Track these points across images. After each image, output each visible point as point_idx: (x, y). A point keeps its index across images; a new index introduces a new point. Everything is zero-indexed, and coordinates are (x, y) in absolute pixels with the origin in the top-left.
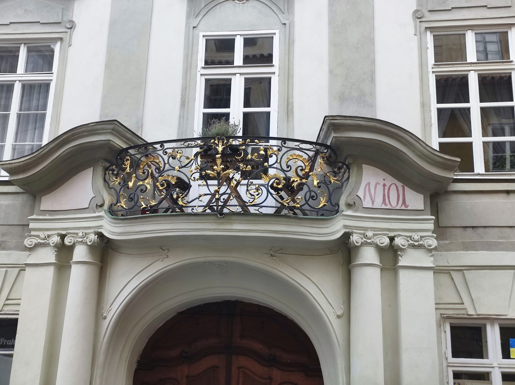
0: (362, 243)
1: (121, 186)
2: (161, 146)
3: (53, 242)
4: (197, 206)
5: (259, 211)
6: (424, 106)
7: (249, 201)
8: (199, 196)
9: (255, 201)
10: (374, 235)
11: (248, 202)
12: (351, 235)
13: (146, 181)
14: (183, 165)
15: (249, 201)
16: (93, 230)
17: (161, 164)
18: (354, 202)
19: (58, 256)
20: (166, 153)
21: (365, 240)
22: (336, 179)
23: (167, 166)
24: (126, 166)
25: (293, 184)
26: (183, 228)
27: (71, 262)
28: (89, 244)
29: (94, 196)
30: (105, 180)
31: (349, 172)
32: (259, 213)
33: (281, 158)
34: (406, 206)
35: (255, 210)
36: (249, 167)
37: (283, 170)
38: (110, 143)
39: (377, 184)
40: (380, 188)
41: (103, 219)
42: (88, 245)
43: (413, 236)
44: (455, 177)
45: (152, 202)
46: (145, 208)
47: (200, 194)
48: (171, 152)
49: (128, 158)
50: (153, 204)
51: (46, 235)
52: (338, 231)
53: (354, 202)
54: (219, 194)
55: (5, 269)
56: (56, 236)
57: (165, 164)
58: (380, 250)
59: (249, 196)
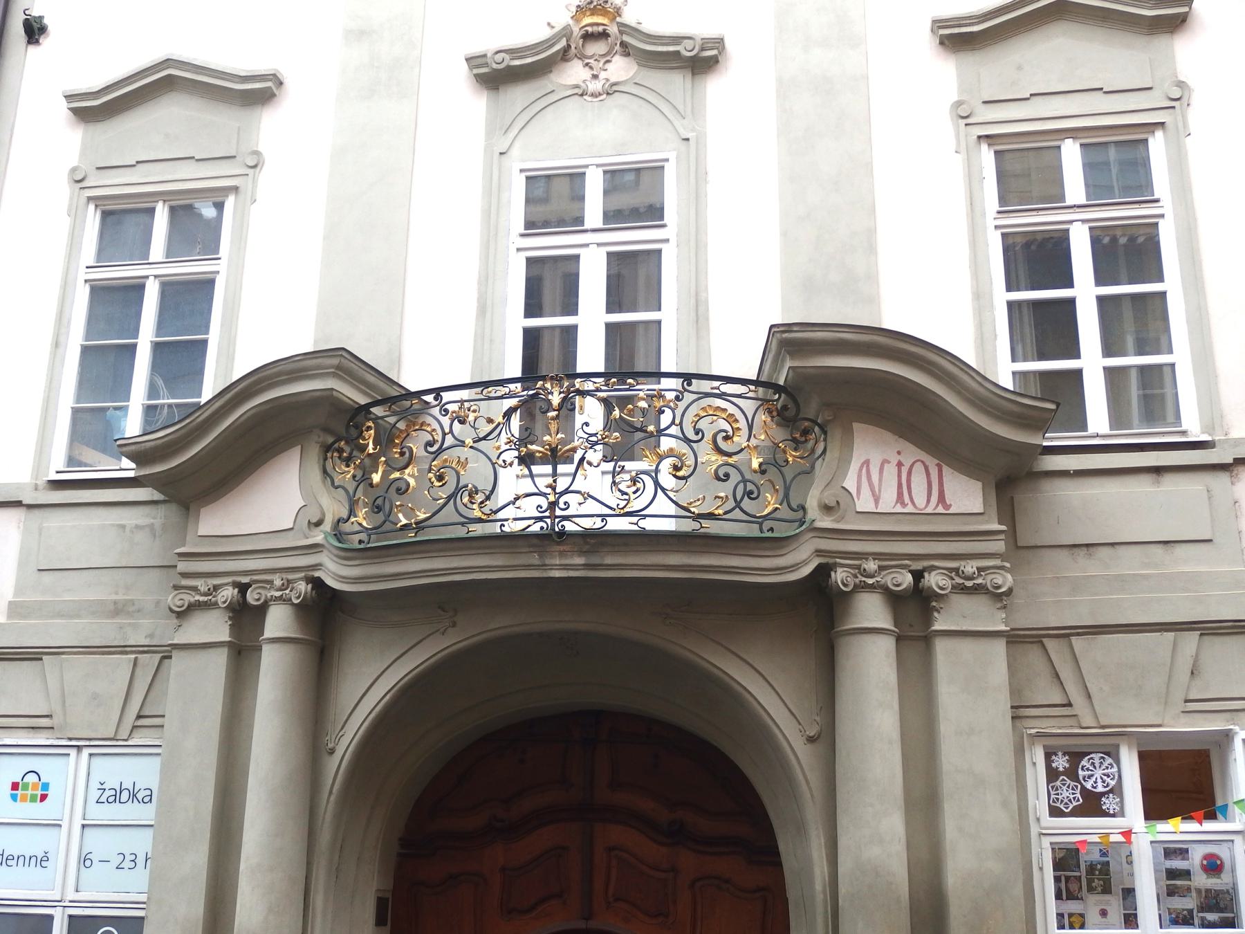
0: (855, 586)
2: (436, 399)
3: (223, 600)
6: (981, 297)
7: (618, 505)
8: (515, 498)
10: (881, 568)
11: (616, 508)
12: (832, 570)
13: (407, 471)
14: (481, 435)
15: (618, 505)
16: (303, 575)
18: (837, 502)
19: (234, 628)
20: (446, 411)
21: (864, 579)
22: (798, 454)
24: (366, 442)
27: (832, 632)
28: (296, 601)
29: (304, 504)
30: (325, 472)
33: (683, 415)
34: (947, 507)
37: (687, 441)
39: (885, 462)
40: (891, 470)
41: (322, 551)
42: (293, 604)
43: (962, 568)
44: (1045, 444)
45: (418, 513)
46: (405, 525)
49: (370, 424)
50: (422, 516)
51: (211, 586)
52: (805, 563)
53: (837, 502)
54: (556, 493)
55: (133, 656)
56: (231, 588)
57: (444, 434)
58: (895, 599)
59: (618, 494)
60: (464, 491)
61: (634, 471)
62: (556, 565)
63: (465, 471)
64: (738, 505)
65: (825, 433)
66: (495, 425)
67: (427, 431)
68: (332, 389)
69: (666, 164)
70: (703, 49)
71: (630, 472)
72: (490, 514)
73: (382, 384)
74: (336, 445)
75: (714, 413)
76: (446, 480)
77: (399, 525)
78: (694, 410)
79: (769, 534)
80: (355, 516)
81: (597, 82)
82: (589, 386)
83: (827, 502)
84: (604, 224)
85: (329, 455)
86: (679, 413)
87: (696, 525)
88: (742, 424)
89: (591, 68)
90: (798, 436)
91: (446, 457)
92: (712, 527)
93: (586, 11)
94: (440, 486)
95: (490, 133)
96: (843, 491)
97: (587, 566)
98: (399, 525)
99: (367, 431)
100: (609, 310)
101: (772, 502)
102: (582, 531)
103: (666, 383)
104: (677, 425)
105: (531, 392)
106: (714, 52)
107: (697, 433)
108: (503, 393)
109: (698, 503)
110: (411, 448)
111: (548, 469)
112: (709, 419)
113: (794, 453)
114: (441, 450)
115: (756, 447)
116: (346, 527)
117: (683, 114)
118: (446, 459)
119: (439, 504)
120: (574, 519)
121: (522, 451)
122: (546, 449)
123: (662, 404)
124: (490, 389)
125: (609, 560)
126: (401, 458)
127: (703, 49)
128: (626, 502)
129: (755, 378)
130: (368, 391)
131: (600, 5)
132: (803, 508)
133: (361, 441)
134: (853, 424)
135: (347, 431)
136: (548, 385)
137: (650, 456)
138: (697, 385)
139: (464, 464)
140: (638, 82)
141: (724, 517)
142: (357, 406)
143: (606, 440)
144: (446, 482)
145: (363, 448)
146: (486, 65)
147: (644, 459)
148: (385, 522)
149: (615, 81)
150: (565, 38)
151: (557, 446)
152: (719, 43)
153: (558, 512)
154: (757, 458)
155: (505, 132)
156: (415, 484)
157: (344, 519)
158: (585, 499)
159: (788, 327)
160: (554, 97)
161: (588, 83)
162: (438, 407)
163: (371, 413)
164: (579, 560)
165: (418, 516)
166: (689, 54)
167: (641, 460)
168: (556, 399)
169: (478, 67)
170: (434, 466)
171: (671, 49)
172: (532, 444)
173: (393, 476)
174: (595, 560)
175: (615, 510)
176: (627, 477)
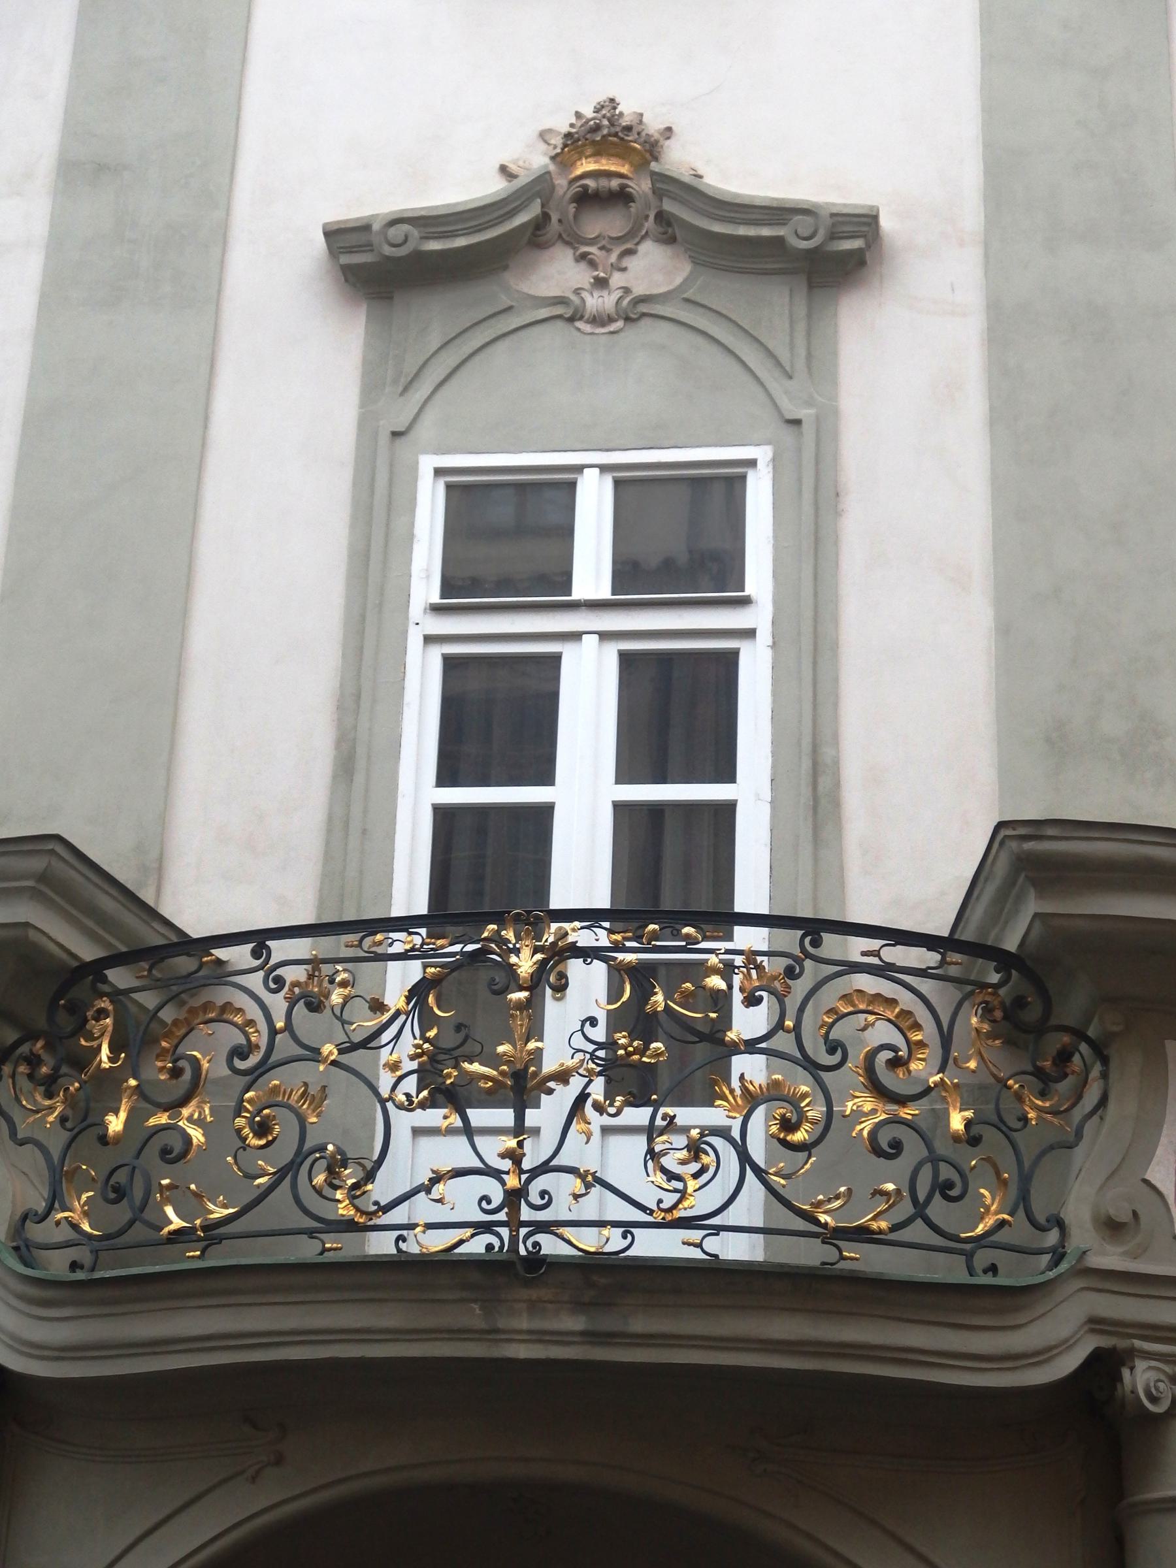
2: (256, 954)
7: (660, 1201)
8: (430, 1180)
9: (686, 1204)
11: (655, 1208)
12: (1123, 1365)
13: (186, 1112)
14: (357, 1038)
15: (660, 1201)
17: (257, 1031)
18: (1135, 1214)
20: (280, 981)
22: (1047, 1104)
24: (95, 1044)
26: (359, 1325)
33: (801, 1010)
36: (657, 1049)
37: (812, 1067)
45: (211, 1206)
46: (179, 1232)
47: (433, 1172)
49: (105, 1004)
50: (219, 1213)
52: (1065, 1346)
53: (1135, 1214)
57: (273, 1032)
59: (660, 1178)
60: (317, 1159)
61: (695, 1127)
62: (520, 1332)
63: (318, 1116)
64: (920, 1211)
65: (1105, 1061)
66: (386, 1017)
67: (235, 1025)
68: (27, 925)
69: (436, 598)
70: (833, 236)
71: (686, 1130)
72: (374, 1213)
73: (130, 919)
74: (24, 1049)
77: (166, 1230)
78: (830, 996)
79: (988, 1280)
80: (64, 1209)
81: (605, 293)
82: (584, 937)
83: (1112, 1212)
84: (613, 594)
87: (830, 1254)
88: (928, 1032)
89: (593, 264)
90: (1047, 1064)
91: (277, 1082)
93: (584, 145)
95: (371, 389)
96: (1146, 1189)
97: (591, 1337)
98: (166, 1230)
99: (97, 1020)
100: (624, 775)
101: (993, 1208)
102: (580, 1256)
103: (748, 938)
104: (788, 1031)
105: (470, 948)
106: (857, 244)
107: (831, 1051)
108: (408, 947)
109: (837, 1204)
111: (505, 1117)
113: (1039, 1103)
114: (264, 1068)
115: (956, 1086)
116: (37, 1233)
117: (788, 368)
118: (275, 1086)
119: (258, 1186)
120: (561, 1230)
121: (449, 1076)
122: (503, 1073)
124: (379, 937)
125: (638, 1325)
126: (174, 1081)
127: (833, 236)
128: (678, 1195)
129: (945, 933)
130: (101, 932)
131: (616, 135)
132: (1060, 1224)
133: (83, 1042)
134: (1167, 1042)
135: (51, 1019)
136: (509, 934)
138: (832, 946)
139: (317, 1099)
140: (693, 298)
141: (892, 1236)
142: (75, 964)
144: (275, 1139)
145: (82, 1061)
146: (368, 247)
147: (718, 1102)
148: (131, 1223)
149: (641, 293)
150: (539, 200)
151: (526, 1068)
152: (869, 224)
153: (526, 1214)
154: (961, 1110)
155: (406, 389)
156: (202, 1139)
157: (36, 1214)
158: (588, 1186)
159: (1036, 828)
160: (515, 321)
161: (585, 295)
162: (261, 974)
163: (105, 980)
164: (574, 1323)
165: (212, 1212)
166: (804, 245)
167: (712, 1105)
168: (525, 963)
169: (350, 250)
171: (766, 232)
173: (152, 1122)
174: (607, 1322)
175: (651, 1212)
176: (680, 1141)
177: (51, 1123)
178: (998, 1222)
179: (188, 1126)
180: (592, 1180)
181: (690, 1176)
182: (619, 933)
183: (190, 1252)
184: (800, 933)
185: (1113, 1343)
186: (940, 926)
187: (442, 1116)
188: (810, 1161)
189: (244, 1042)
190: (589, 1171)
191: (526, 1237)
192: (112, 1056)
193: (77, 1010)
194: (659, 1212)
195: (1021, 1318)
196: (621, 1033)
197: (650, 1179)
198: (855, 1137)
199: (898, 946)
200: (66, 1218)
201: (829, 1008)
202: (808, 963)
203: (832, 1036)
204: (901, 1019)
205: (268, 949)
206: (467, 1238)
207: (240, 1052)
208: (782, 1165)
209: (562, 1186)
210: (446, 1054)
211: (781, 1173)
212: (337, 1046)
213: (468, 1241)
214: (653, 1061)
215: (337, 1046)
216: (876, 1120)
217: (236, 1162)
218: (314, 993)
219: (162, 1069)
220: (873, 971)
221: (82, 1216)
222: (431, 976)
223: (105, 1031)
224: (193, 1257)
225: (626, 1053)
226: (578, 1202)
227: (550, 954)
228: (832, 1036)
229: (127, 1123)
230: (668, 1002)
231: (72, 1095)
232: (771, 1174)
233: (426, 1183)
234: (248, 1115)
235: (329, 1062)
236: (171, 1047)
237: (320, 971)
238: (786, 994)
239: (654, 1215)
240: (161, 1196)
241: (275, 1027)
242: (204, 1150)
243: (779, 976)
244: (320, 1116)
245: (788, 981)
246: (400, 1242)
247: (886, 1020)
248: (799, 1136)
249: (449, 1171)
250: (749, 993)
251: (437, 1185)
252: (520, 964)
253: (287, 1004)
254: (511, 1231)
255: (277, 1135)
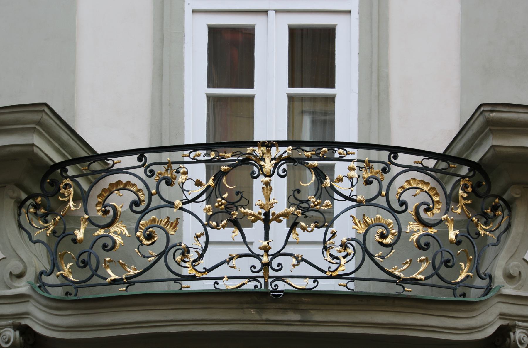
1: (58, 237)
2: (140, 159)
4: (226, 276)
5: (347, 288)
7: (330, 268)
8: (229, 258)
9: (340, 269)
11: (327, 270)
12: (511, 331)
13: (112, 229)
14: (190, 198)
15: (330, 268)
16: (11, 322)
17: (143, 194)
18: (520, 273)
20: (152, 172)
22: (487, 228)
23: (155, 198)
24: (66, 199)
25: (412, 237)
26: (201, 318)
29: (3, 256)
30: (20, 226)
31: (510, 216)
32: (348, 290)
33: (389, 187)
35: (339, 285)
36: (327, 203)
37: (393, 211)
38: (33, 150)
41: (28, 301)
45: (129, 270)
47: (230, 255)
48: (163, 171)
50: (132, 272)
52: (490, 324)
53: (520, 273)
54: (269, 255)
56: (11, 330)
57: (151, 195)
59: (330, 259)
63: (174, 231)
65: (510, 210)
68: (33, 145)
72: (204, 272)
75: (417, 186)
76: (155, 239)
79: (462, 299)
80: (59, 271)
83: (511, 272)
85: (24, 210)
86: (385, 184)
92: (410, 290)
94: (150, 245)
104: (383, 196)
110: (115, 206)
112: (413, 191)
115: (452, 220)
116: (46, 279)
118: (154, 219)
119: (150, 261)
121: (234, 214)
123: (370, 175)
124: (199, 152)
128: (338, 265)
132: (490, 277)
133: (60, 199)
135: (42, 188)
137: (359, 224)
141: (425, 282)
142: (52, 164)
143: (318, 207)
144: (155, 241)
148: (92, 276)
162: (143, 169)
164: (297, 317)
165: (129, 272)
170: (142, 225)
172: (243, 207)
175: (326, 272)
177: (49, 234)
178: (467, 276)
179: (114, 236)
180: (300, 260)
181: (342, 257)
182: (309, 152)
183: (120, 288)
184: (389, 152)
185: (508, 323)
186: (440, 150)
187: (232, 231)
188: (392, 251)
189: (137, 199)
190: (299, 255)
191: (271, 283)
192: (75, 204)
193: (55, 183)
194: (329, 272)
195: (474, 314)
196: (311, 196)
197: (326, 258)
198: (410, 241)
199: (430, 159)
200: (61, 274)
201: (401, 186)
202: (392, 166)
203: (401, 198)
204: (430, 191)
205: (145, 157)
206: (246, 283)
207: (136, 203)
208: (381, 252)
209: (287, 262)
210: (231, 205)
211: (380, 256)
212: (181, 201)
213: (247, 284)
214: (326, 208)
215: (181, 201)
216: (419, 234)
217: (139, 251)
218: (169, 177)
219: (98, 211)
220: (418, 170)
221: (68, 273)
222: (224, 170)
223: (70, 194)
224: (122, 290)
225: (314, 205)
226: (295, 268)
227: (279, 161)
228: (401, 198)
229: (85, 234)
230: (332, 183)
231: (57, 222)
232: (376, 256)
233: (227, 260)
234: (142, 231)
235: (178, 208)
236: (102, 201)
237: (171, 167)
238: (382, 180)
239: (327, 273)
240: (105, 265)
241: (152, 192)
242: (123, 246)
243: (379, 172)
244: (176, 231)
245: (383, 174)
246: (216, 284)
247: (424, 191)
248: (388, 241)
249: (236, 255)
250: (366, 179)
251: (232, 261)
252: (265, 165)
253: (157, 182)
254: (265, 280)
255: (157, 239)
